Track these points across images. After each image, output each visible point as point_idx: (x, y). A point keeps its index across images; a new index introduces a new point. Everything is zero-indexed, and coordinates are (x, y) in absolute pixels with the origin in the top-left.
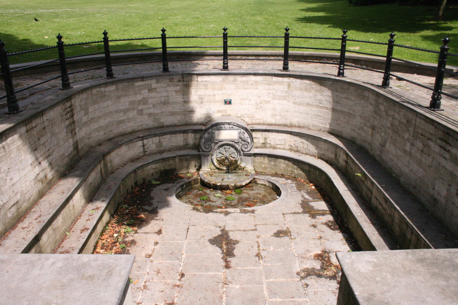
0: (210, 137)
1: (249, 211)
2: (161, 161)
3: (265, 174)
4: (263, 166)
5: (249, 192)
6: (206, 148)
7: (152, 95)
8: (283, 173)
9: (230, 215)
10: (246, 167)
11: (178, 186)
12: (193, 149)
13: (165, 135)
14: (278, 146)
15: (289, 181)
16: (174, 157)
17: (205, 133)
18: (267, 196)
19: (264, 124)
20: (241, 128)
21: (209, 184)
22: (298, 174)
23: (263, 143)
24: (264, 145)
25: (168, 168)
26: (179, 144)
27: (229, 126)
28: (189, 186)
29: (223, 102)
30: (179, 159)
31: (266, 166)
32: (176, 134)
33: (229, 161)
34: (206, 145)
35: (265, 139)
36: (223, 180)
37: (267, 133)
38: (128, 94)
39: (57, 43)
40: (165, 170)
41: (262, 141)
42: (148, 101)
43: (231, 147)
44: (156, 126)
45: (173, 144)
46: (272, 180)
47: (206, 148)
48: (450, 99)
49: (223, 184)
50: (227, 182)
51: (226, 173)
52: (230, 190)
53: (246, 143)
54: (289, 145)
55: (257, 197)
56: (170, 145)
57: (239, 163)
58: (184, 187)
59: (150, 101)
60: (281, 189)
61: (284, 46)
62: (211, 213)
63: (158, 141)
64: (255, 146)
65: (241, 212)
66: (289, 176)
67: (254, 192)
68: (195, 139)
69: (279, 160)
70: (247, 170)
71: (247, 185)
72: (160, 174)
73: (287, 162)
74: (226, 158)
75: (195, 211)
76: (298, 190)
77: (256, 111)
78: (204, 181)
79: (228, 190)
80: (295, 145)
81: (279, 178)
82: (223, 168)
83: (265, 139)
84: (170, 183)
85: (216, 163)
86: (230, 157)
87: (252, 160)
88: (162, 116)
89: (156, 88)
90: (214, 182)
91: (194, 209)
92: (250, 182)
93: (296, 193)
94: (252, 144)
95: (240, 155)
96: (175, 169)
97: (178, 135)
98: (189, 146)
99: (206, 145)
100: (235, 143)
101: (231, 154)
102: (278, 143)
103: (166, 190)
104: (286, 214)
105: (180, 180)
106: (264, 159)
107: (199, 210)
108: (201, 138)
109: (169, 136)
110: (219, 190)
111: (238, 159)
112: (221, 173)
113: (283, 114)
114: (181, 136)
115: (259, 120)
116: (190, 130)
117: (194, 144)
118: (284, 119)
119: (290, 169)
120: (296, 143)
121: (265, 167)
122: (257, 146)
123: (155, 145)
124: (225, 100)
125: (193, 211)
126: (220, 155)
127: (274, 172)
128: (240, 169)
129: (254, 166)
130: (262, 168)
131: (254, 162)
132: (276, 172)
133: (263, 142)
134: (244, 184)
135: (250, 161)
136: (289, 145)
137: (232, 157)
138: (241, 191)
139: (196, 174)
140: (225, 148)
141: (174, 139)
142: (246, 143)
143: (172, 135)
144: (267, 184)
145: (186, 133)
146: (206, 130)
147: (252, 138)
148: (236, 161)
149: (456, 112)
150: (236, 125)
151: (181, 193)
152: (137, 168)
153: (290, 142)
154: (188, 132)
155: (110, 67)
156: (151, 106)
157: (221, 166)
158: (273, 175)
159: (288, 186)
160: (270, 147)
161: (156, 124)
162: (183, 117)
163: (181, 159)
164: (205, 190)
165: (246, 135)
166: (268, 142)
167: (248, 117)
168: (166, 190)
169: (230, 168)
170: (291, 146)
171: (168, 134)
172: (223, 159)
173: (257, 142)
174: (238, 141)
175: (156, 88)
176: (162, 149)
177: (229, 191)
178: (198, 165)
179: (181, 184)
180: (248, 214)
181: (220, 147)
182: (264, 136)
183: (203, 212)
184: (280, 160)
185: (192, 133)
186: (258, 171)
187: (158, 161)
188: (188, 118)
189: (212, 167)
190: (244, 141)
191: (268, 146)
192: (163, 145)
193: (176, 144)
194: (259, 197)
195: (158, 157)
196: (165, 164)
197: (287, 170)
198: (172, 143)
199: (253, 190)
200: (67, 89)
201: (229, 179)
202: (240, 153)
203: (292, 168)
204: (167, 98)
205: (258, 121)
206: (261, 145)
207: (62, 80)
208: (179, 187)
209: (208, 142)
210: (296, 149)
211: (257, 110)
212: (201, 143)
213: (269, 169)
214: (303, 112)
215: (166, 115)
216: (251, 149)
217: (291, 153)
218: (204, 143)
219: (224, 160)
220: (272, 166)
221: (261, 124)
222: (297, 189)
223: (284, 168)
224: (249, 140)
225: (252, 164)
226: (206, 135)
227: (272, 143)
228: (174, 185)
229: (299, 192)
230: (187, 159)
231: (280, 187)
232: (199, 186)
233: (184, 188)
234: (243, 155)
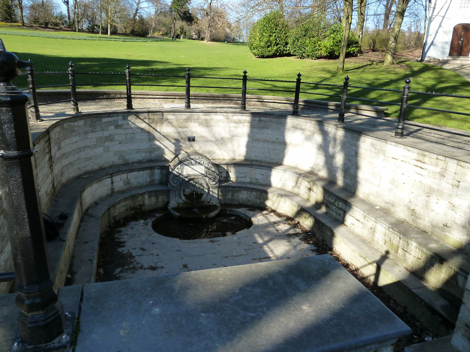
7: (119, 131)
38: (95, 130)
42: (114, 138)
47: (175, 183)
48: (358, 177)
59: (117, 137)
89: (123, 125)
99: (174, 181)
123: (122, 182)
124: (189, 137)
149: (295, 1)
156: (117, 142)
161: (121, 162)
162: (148, 154)
175: (123, 125)
195: (127, 195)
204: (133, 135)
218: (173, 179)
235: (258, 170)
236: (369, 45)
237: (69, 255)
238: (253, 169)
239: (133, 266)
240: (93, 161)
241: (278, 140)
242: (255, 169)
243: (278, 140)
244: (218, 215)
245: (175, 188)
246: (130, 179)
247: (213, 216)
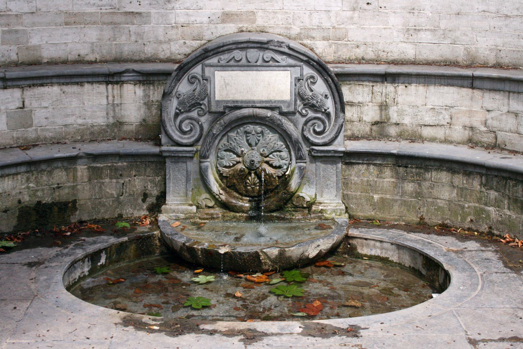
0: (196, 93)
1: (339, 329)
2: (23, 169)
3: (383, 224)
4: (376, 197)
5: (330, 280)
6: (184, 133)
8: (447, 222)
9: (266, 340)
10: (319, 199)
11: (80, 253)
12: (137, 140)
13: (42, 85)
14: (426, 132)
15: (472, 245)
16: (72, 160)
17: (178, 79)
18: (396, 291)
19: (377, 62)
20: (302, 61)
21: (191, 250)
22: (501, 223)
23: (376, 123)
25: (47, 200)
26: (90, 121)
27: (261, 54)
28: (117, 261)
30: (89, 168)
31: (388, 196)
32: (81, 84)
33: (259, 177)
34: (181, 122)
35: (383, 107)
36: (237, 239)
37: (389, 88)
40: (39, 203)
43: (267, 131)
44: (14, 57)
45: (70, 120)
46: (409, 240)
49: (241, 249)
50: (253, 245)
51: (250, 219)
52: (264, 272)
53: (319, 115)
54: (465, 127)
55: (361, 293)
56: (60, 121)
57: (294, 184)
58: (103, 261)
60: (446, 267)
62: (193, 335)
63: (19, 104)
64: (349, 133)
65: (307, 332)
66: (469, 229)
67: (349, 279)
68: (148, 105)
69: (434, 173)
70: (321, 211)
71: (321, 257)
72: (20, 218)
73: (459, 180)
74: (252, 168)
75: (131, 329)
76: (511, 268)
77: (352, 18)
78: (171, 240)
79: (255, 272)
80: (485, 124)
81: (435, 237)
82: (240, 203)
83: (383, 107)
84: (50, 246)
85: (215, 188)
86: (265, 166)
87: (341, 177)
88: (34, 24)
90: (206, 245)
91: (126, 322)
92: (332, 251)
93: (504, 277)
94: (341, 121)
95: (300, 158)
96: (75, 202)
97: (87, 86)
98: (126, 128)
99: (181, 122)
100: (282, 113)
101: (266, 152)
102: (428, 119)
103: (30, 265)
104: (483, 341)
105: (86, 239)
106: (381, 172)
107: (146, 324)
109: (56, 89)
110: (226, 272)
111: (292, 172)
112: (231, 220)
113: (442, 27)
114: (100, 93)
115: (362, 48)
116: (127, 71)
117: (141, 124)
118: (448, 41)
119: (470, 205)
120: (489, 116)
121: (382, 200)
122: (357, 133)
125: (120, 328)
126: (229, 158)
127: (416, 219)
128: (297, 208)
129: (345, 198)
130: (374, 206)
131: (346, 184)
132: (422, 218)
133: (377, 118)
134: (312, 253)
135: (334, 179)
136: (465, 127)
137: (271, 166)
138: (307, 276)
139: (148, 221)
140: (246, 133)
141: (75, 103)
142: (319, 115)
143: (65, 88)
144: (394, 256)
145: (117, 83)
148: (285, 180)
150: (286, 50)
151: (89, 280)
153: (470, 113)
154: (123, 79)
157: (234, 197)
158: (409, 228)
159: (472, 258)
160: (400, 136)
162: (107, 33)
163: (98, 168)
164: (174, 274)
166: (394, 117)
167: (324, 39)
168: (30, 265)
169: (263, 204)
170: (472, 128)
171: (52, 84)
172: (241, 171)
173: (355, 117)
174: (292, 109)
176: (31, 134)
177: (259, 274)
178: (155, 192)
179: (91, 249)
180: (335, 339)
181: (232, 130)
182: (379, 99)
183: (159, 331)
184: (433, 175)
185: (136, 83)
186: (360, 214)
187: (13, 171)
188: (124, 38)
189: (204, 198)
190: (313, 107)
191: (393, 131)
192: (35, 122)
193: (80, 121)
194: (369, 295)
196: (37, 183)
197: (463, 207)
198: (67, 116)
199: (343, 274)
201: (260, 235)
202: (299, 149)
203: (479, 200)
205: (358, 50)
206: (368, 129)
208: (83, 260)
209: (189, 111)
210: (488, 139)
211: (356, 14)
212: (164, 115)
213: (396, 208)
214: (515, 13)
215: (49, 24)
216: (336, 137)
217: (472, 151)
218: (177, 115)
219: (242, 176)
220: (406, 198)
221: (369, 62)
222: (506, 266)
223: (450, 201)
224: (330, 105)
225: (337, 188)
227: (407, 121)
228: (66, 251)
229: (515, 275)
230: (116, 169)
231: (441, 259)
232: (157, 260)
233: (102, 266)
234: (308, 159)
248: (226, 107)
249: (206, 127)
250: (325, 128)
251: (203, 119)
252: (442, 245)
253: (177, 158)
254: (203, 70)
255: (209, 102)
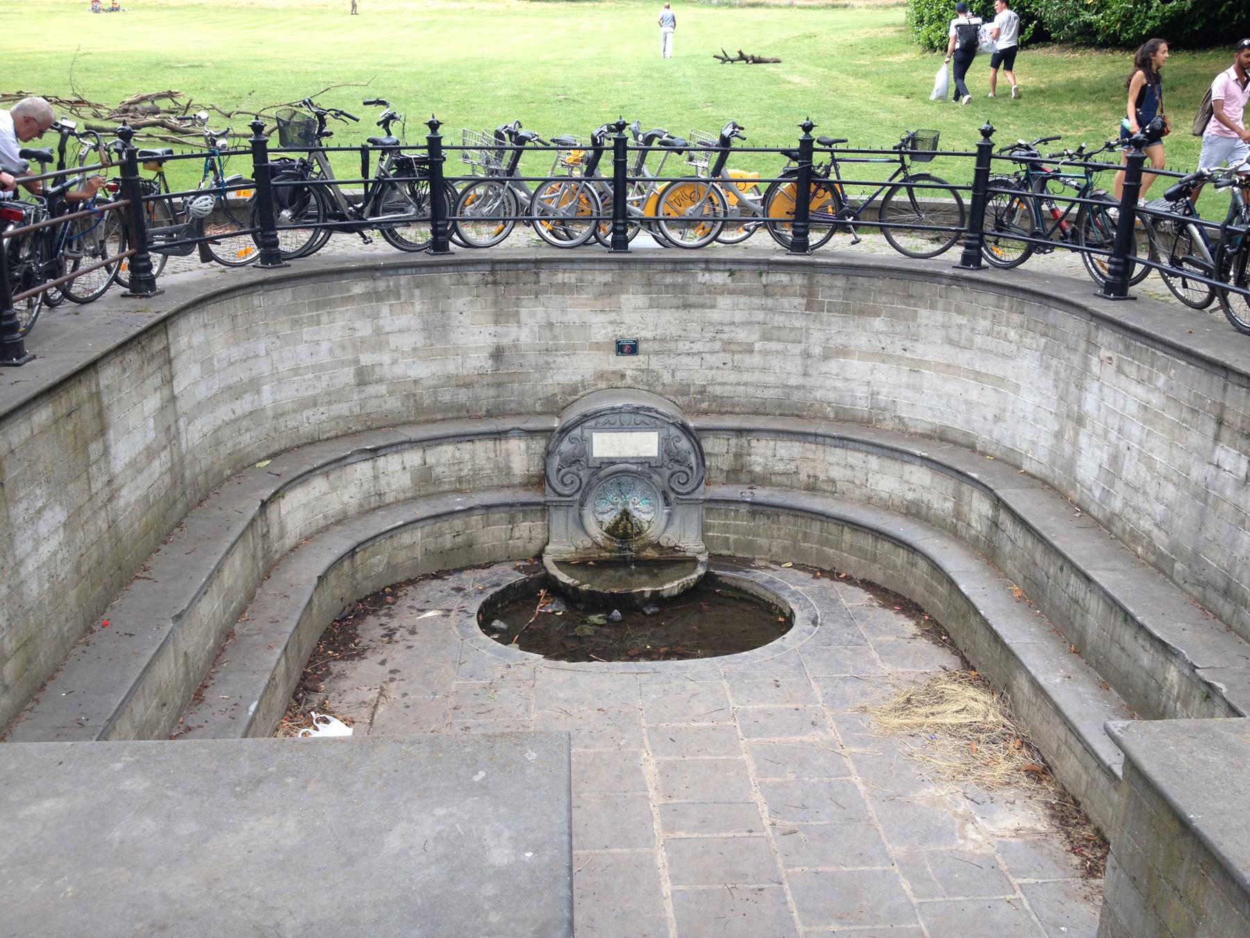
0: (576, 452)
17: (560, 440)
24: (736, 474)
29: (614, 346)
34: (563, 477)
39: (978, 145)
41: (726, 463)
53: (683, 468)
61: (992, 160)
108: (548, 453)
124: (618, 342)
142: (683, 468)
143: (460, 446)
146: (565, 431)
147: (701, 455)
152: (359, 545)
155: (272, 233)
165: (684, 444)
195: (423, 510)
200: (148, 296)
207: (433, 232)
218: (559, 470)
224: (693, 459)
226: (566, 446)
235: (838, 451)
236: (121, 581)
237: (186, 680)
238: (820, 447)
239: (1092, 881)
240: (322, 410)
241: (908, 355)
242: (828, 449)
243: (908, 355)
244: (689, 593)
245: (567, 499)
246: (430, 468)
247: (675, 592)
248: (602, 463)
249: (585, 481)
250: (688, 480)
251: (581, 473)
252: (1088, 749)
253: (558, 505)
254: (582, 432)
255: (587, 460)
